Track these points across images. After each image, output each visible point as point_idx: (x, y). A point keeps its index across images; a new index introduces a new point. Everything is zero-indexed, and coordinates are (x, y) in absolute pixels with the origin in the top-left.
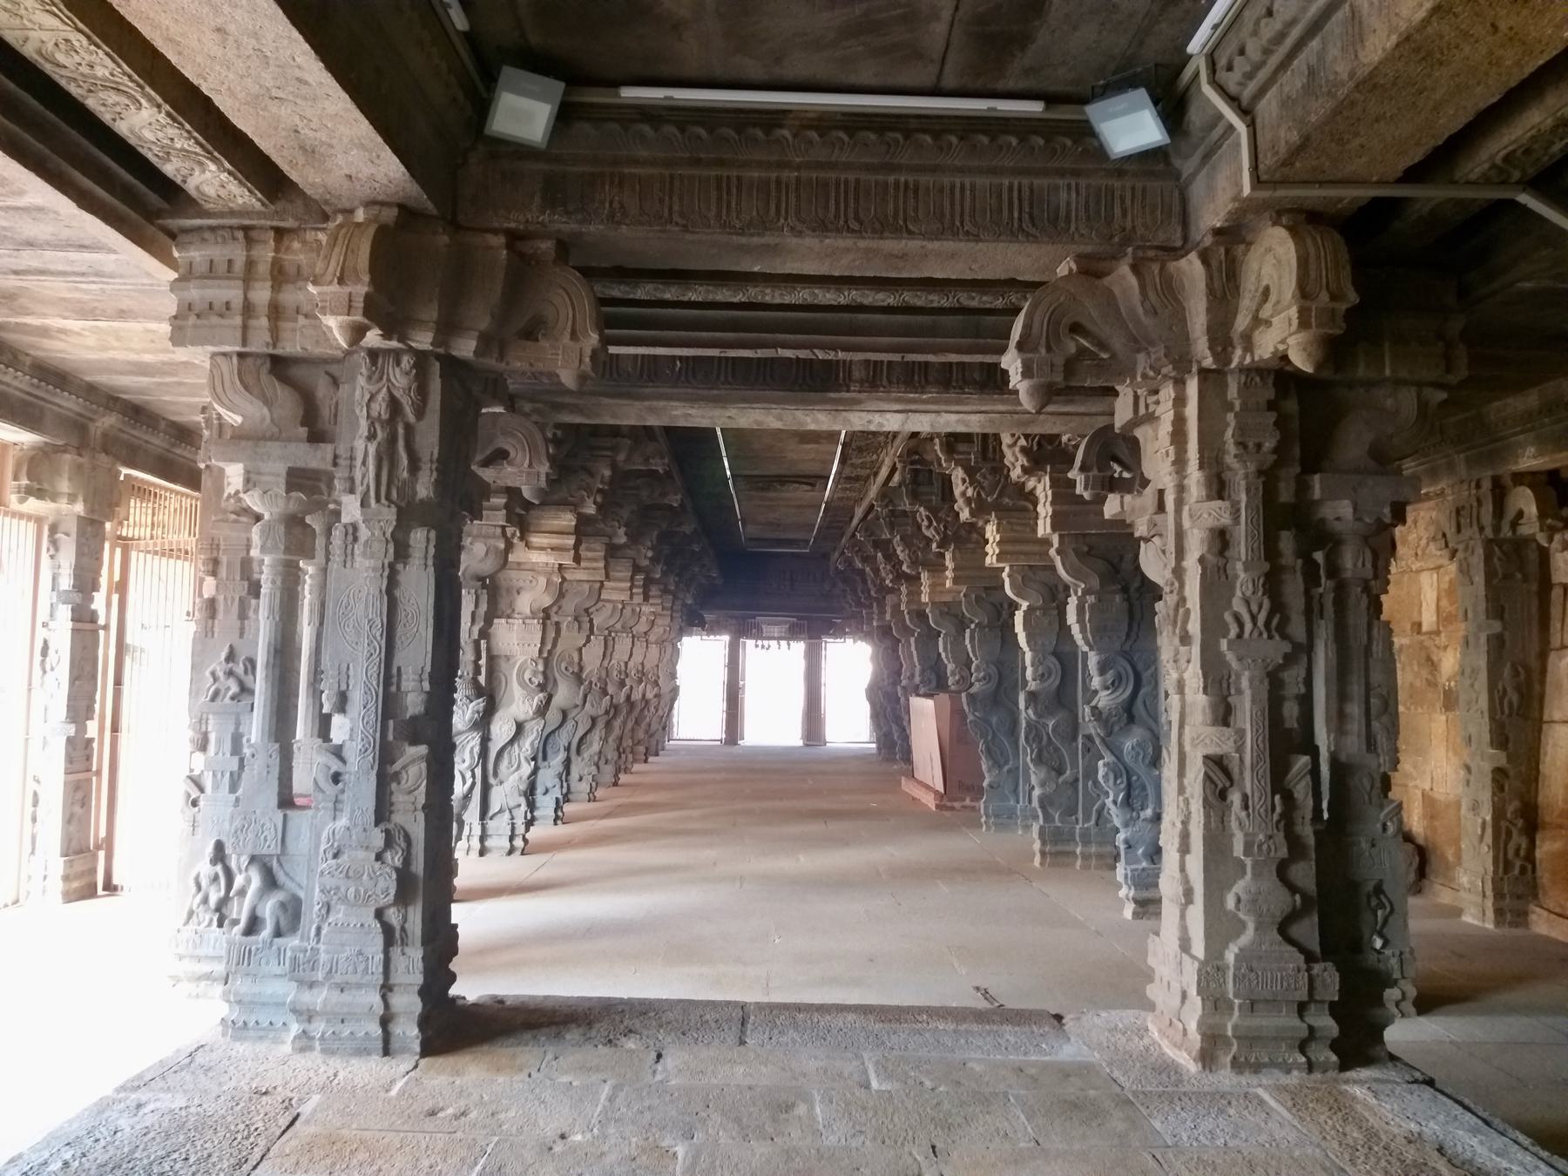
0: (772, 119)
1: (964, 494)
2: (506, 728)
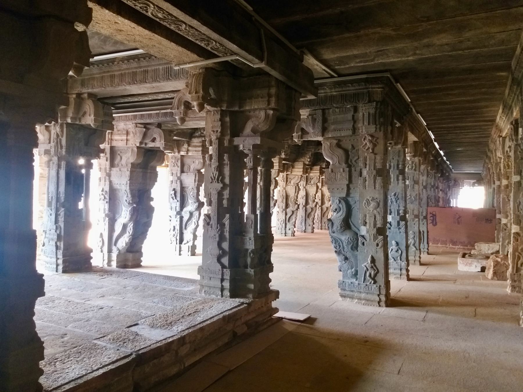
0: (113, 60)
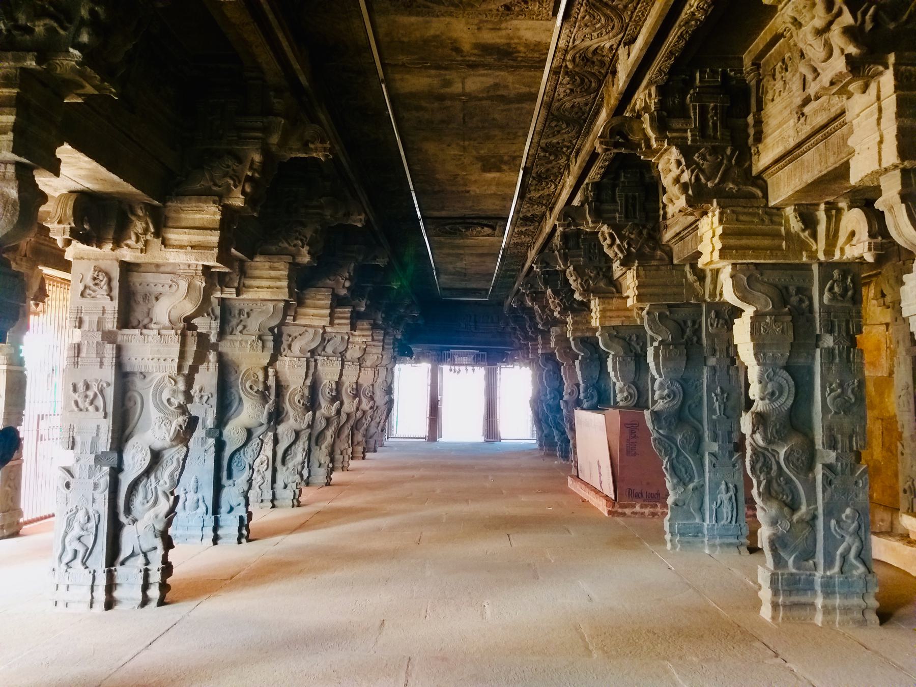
1: (677, 180)
2: (139, 456)
